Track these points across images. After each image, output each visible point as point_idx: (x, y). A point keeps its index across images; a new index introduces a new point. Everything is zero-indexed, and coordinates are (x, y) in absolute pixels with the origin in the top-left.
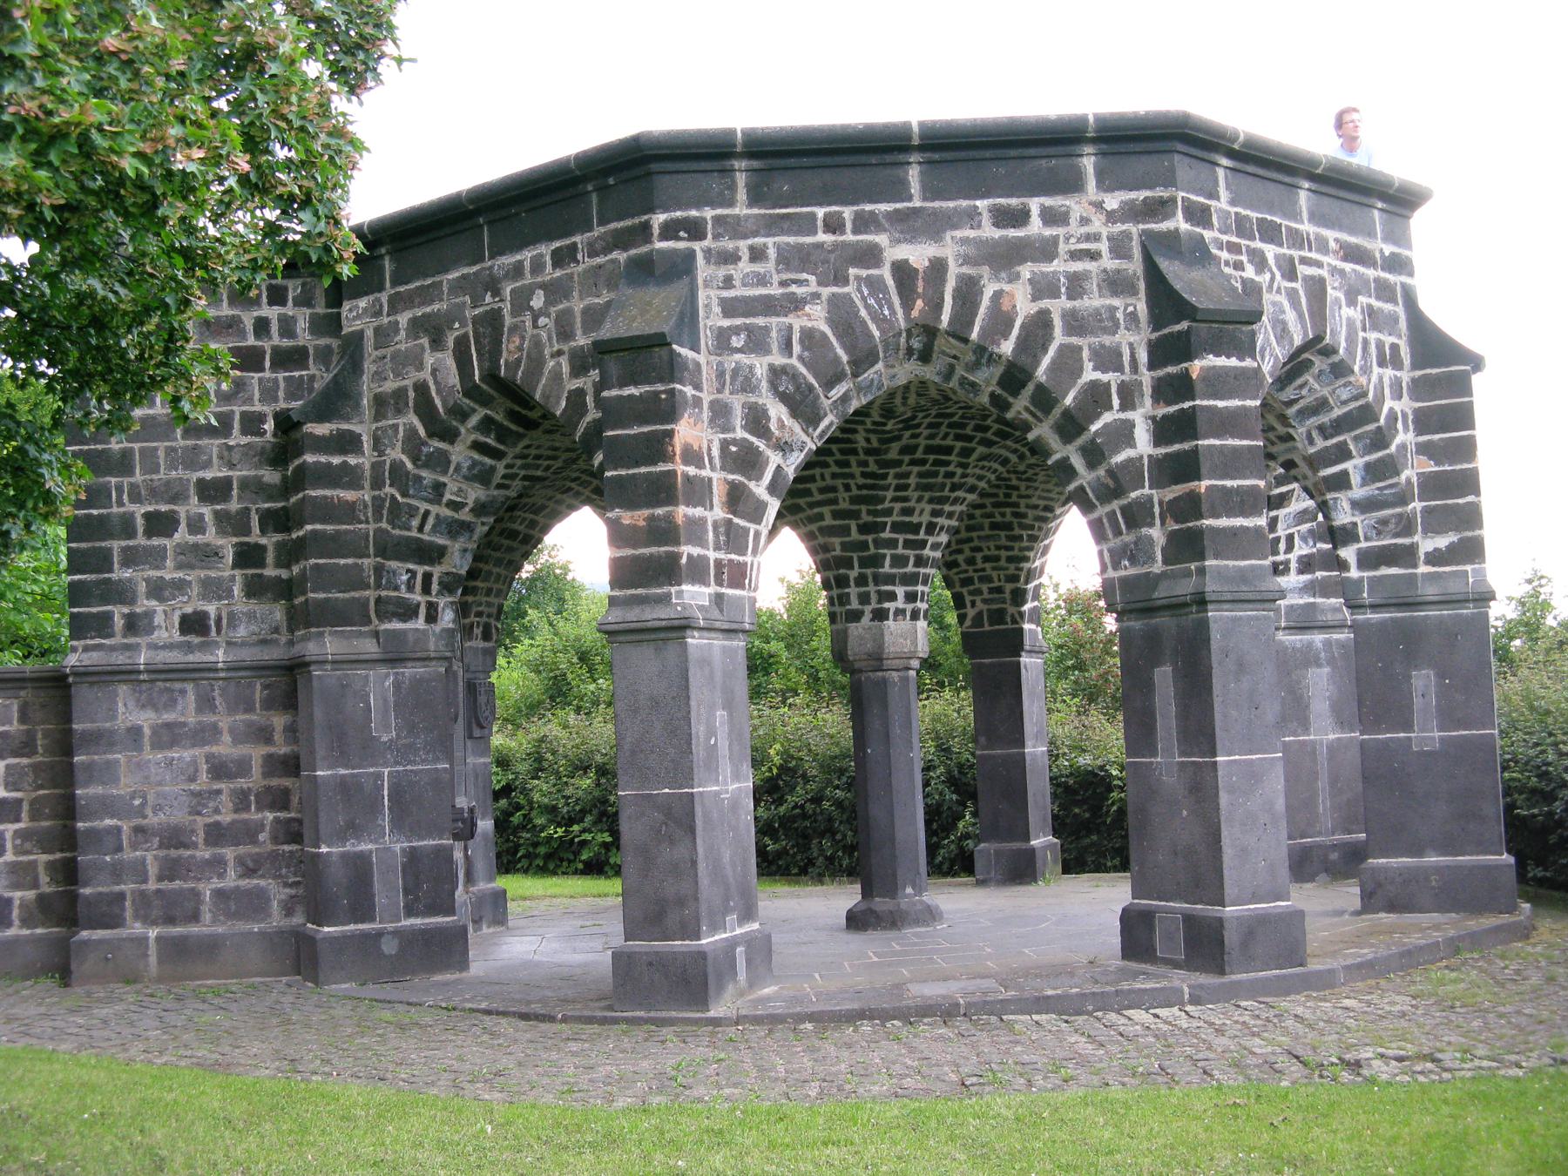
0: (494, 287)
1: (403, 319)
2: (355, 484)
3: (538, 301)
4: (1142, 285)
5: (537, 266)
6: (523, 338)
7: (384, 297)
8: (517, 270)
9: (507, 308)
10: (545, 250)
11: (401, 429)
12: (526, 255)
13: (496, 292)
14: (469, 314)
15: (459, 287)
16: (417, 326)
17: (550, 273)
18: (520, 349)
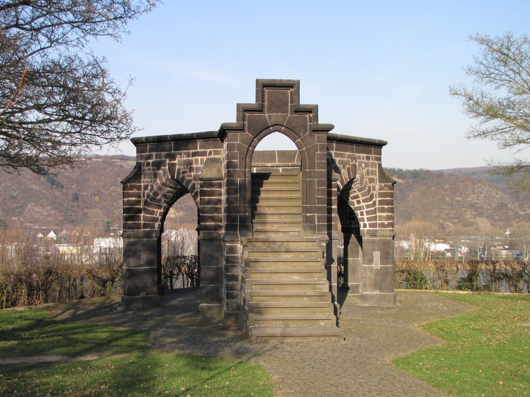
2: (380, 216)
10: (365, 155)
12: (361, 155)
15: (349, 156)
17: (365, 161)
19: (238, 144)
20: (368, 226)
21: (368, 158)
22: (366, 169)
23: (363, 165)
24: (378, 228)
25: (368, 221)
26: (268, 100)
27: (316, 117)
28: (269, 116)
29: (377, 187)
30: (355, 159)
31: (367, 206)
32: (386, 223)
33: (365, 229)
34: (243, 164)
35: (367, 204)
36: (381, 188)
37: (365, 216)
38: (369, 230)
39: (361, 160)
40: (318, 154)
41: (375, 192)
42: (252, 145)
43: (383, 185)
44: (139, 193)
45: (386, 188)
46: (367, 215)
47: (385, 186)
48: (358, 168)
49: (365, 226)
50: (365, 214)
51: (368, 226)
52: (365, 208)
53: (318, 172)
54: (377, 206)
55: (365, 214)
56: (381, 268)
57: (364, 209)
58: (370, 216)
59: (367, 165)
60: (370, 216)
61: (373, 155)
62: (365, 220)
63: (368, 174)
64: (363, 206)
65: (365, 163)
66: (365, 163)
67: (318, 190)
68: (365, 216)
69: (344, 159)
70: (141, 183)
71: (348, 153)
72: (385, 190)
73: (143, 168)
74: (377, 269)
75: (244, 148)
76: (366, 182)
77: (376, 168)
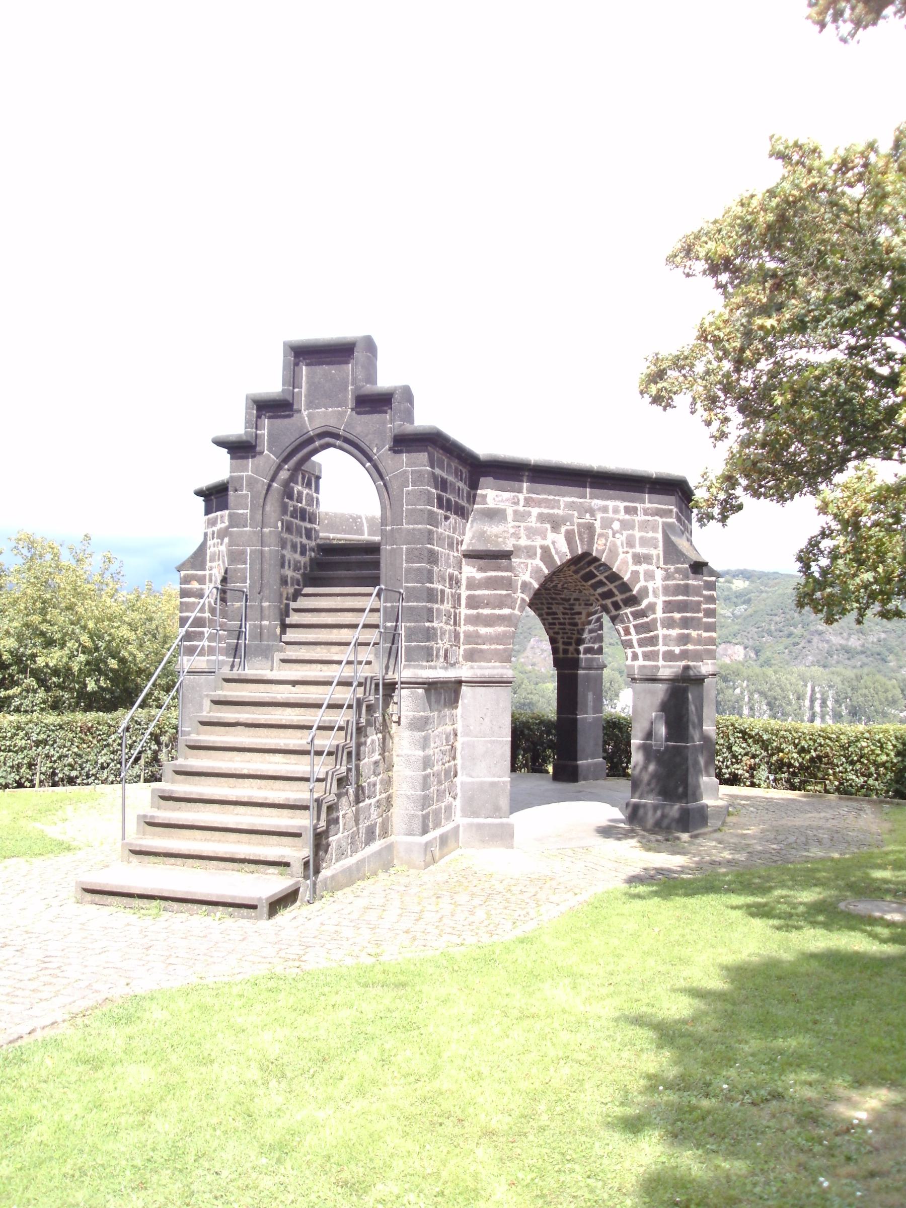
0: (592, 513)
1: (535, 511)
3: (616, 526)
4: (661, 544)
5: (616, 511)
6: (607, 541)
7: (521, 497)
8: (605, 509)
9: (597, 524)
10: (621, 505)
11: (529, 566)
12: (611, 504)
13: (593, 515)
14: (576, 521)
15: (571, 506)
16: (542, 518)
17: (622, 515)
18: (605, 545)
19: (249, 478)
20: (640, 657)
21: (634, 511)
22: (625, 533)
23: (616, 526)
24: (661, 662)
25: (640, 646)
26: (307, 383)
27: (409, 416)
28: (309, 416)
29: (659, 574)
30: (592, 513)
31: (636, 615)
32: (677, 650)
33: (637, 664)
34: (259, 517)
35: (633, 609)
36: (668, 577)
37: (634, 637)
38: (644, 666)
39: (610, 515)
40: (408, 493)
41: (650, 585)
42: (278, 478)
43: (672, 568)
44: (202, 589)
45: (677, 575)
46: (637, 633)
47: (677, 571)
48: (598, 530)
49: (635, 657)
50: (632, 630)
51: (640, 657)
52: (631, 618)
53: (408, 530)
54: (659, 614)
55: (632, 630)
56: (667, 747)
57: (629, 621)
58: (643, 636)
59: (625, 525)
60: (643, 636)
61: (648, 505)
62: (635, 644)
63: (630, 543)
64: (626, 614)
65: (622, 522)
66: (622, 522)
67: (408, 571)
68: (634, 637)
69: (556, 511)
70: (205, 570)
71: (567, 499)
72: (675, 579)
73: (209, 543)
74: (658, 751)
75: (259, 485)
76: (625, 563)
77: (658, 532)
